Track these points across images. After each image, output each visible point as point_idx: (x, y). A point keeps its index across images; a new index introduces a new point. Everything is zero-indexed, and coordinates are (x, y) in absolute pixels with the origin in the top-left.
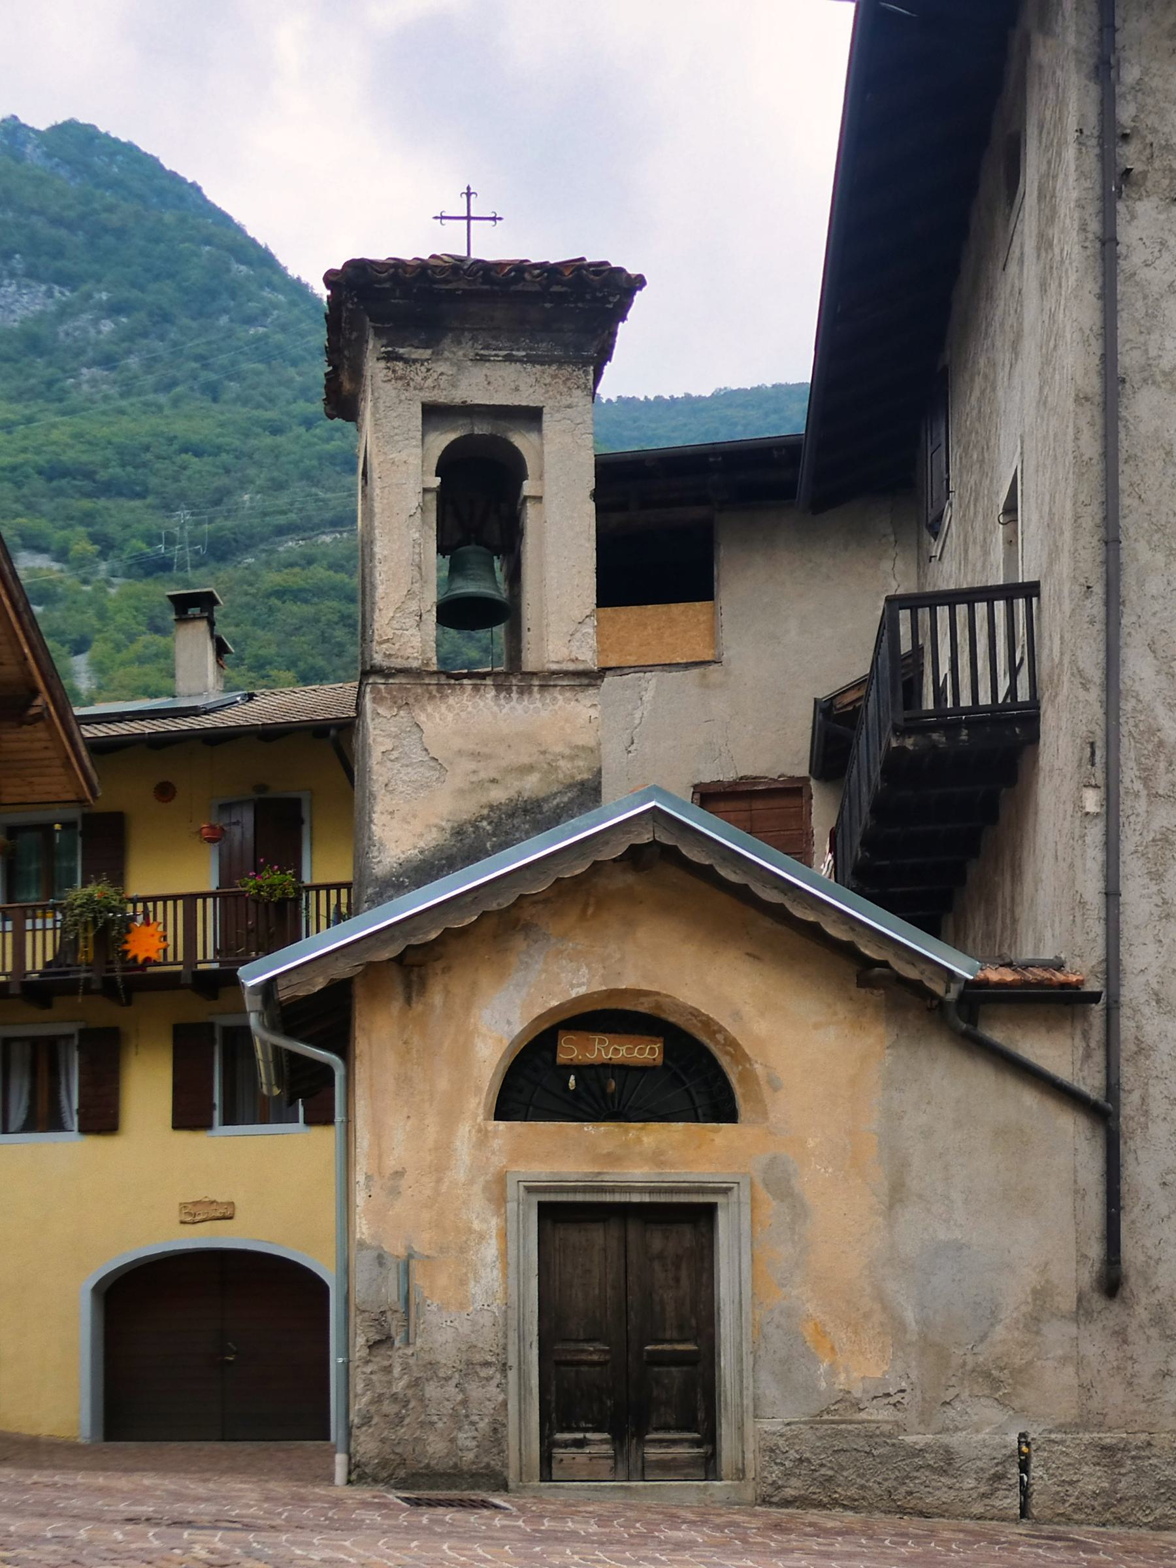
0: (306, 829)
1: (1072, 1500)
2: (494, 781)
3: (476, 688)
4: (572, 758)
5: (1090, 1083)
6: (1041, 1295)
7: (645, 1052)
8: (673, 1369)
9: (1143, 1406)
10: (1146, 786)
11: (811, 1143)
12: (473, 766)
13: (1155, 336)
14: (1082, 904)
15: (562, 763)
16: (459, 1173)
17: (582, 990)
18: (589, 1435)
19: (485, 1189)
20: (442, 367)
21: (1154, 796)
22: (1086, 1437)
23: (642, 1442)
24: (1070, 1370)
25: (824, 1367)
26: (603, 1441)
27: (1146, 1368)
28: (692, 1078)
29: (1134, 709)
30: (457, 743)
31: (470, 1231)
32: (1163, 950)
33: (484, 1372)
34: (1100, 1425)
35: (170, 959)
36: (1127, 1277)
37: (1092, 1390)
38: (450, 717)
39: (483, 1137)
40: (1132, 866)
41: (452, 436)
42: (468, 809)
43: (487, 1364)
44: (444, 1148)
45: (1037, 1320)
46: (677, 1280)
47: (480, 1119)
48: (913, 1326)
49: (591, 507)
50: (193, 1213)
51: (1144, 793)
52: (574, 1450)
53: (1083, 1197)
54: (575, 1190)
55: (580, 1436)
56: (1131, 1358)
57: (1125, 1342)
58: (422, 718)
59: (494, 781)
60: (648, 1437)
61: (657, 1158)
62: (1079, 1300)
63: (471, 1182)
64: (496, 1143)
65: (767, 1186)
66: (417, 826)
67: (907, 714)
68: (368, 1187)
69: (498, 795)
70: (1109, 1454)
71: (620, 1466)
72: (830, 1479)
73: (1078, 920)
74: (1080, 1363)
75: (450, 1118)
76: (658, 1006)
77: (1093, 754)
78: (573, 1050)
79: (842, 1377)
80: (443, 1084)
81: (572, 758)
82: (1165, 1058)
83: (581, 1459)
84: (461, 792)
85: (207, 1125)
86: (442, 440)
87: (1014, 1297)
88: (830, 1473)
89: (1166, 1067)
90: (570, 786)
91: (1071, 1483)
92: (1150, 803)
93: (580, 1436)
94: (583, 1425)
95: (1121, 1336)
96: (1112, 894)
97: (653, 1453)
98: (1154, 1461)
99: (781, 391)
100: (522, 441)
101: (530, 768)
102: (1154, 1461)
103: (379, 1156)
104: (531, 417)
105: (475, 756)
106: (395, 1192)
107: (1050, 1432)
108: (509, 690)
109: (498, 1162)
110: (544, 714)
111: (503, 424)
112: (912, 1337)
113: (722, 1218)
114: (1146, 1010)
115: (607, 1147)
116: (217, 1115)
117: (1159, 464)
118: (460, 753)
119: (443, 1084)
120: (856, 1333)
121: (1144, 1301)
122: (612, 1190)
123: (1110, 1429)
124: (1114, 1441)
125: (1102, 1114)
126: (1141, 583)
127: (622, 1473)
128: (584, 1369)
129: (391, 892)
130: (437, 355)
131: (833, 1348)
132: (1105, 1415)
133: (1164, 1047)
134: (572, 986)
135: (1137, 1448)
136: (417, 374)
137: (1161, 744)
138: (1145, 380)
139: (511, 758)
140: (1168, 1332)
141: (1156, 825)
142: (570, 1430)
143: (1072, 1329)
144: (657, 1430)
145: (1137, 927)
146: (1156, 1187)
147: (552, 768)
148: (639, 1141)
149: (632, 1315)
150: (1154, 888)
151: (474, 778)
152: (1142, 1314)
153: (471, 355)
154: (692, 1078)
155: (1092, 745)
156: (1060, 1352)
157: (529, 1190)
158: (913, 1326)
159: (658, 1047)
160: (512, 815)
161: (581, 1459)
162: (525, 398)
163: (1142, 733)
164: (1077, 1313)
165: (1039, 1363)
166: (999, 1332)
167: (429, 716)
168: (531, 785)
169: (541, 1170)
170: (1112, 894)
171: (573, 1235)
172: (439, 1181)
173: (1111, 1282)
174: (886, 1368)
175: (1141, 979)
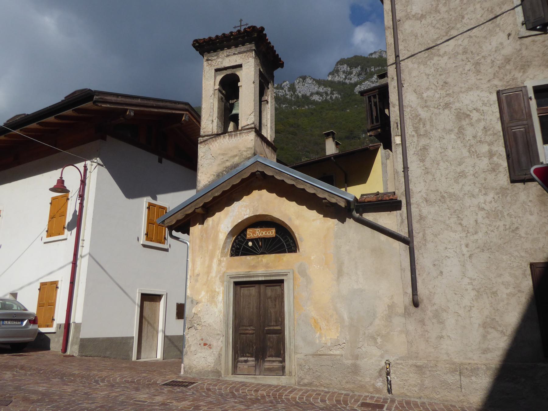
1: (407, 387)
2: (227, 160)
3: (224, 137)
4: (246, 151)
5: (404, 233)
6: (391, 307)
7: (271, 233)
8: (274, 335)
9: (433, 350)
10: (416, 133)
11: (312, 258)
12: (222, 157)
13: (409, 7)
14: (397, 172)
16: (213, 274)
17: (247, 216)
18: (249, 359)
20: (220, 60)
21: (419, 136)
22: (411, 362)
23: (264, 361)
24: (404, 336)
26: (252, 361)
28: (283, 240)
29: (410, 110)
31: (215, 291)
32: (427, 184)
33: (218, 337)
34: (417, 357)
36: (423, 300)
37: (413, 344)
39: (220, 262)
41: (223, 76)
42: (221, 169)
43: (218, 334)
44: (210, 267)
45: (390, 317)
46: (275, 305)
47: (219, 257)
51: (416, 135)
52: (244, 363)
53: (404, 272)
54: (243, 277)
55: (246, 359)
56: (427, 331)
57: (424, 325)
59: (227, 160)
60: (266, 359)
61: (267, 266)
62: (405, 309)
63: (216, 276)
64: (223, 264)
65: (299, 273)
66: (208, 175)
67: (372, 125)
68: (190, 279)
69: (228, 164)
70: (420, 369)
71: (257, 369)
72: (319, 376)
73: (396, 178)
74: (407, 333)
77: (397, 126)
78: (252, 233)
79: (324, 338)
80: (210, 247)
81: (246, 151)
82: (431, 220)
83: (246, 367)
84: (219, 165)
86: (219, 78)
87: (381, 309)
88: (319, 374)
89: (431, 224)
91: (406, 380)
92: (418, 138)
93: (246, 359)
94: (247, 355)
95: (422, 322)
96: (406, 169)
97: (267, 365)
98: (438, 372)
101: (236, 156)
102: (438, 372)
104: (240, 66)
106: (197, 281)
107: (397, 360)
108: (232, 136)
111: (234, 70)
113: (285, 284)
114: (423, 205)
115: (253, 263)
117: (414, 40)
118: (219, 154)
119: (210, 247)
120: (328, 322)
121: (430, 309)
122: (253, 277)
123: (421, 359)
124: (421, 364)
126: (410, 73)
127: (257, 373)
128: (248, 335)
130: (218, 57)
131: (320, 328)
132: (418, 353)
133: (430, 217)
134: (245, 215)
135: (431, 367)
136: (214, 63)
137: (420, 119)
138: (407, 19)
139: (231, 154)
140: (441, 321)
141: (421, 144)
142: (243, 356)
143: (403, 320)
144: (269, 357)
145: (417, 178)
146: (431, 266)
147: (242, 155)
148: (262, 260)
149: (261, 318)
150: (422, 164)
151: (222, 160)
152: (429, 313)
153: (226, 55)
154: (283, 240)
155: (397, 123)
156: (399, 329)
157: (231, 278)
159: (274, 231)
161: (246, 367)
163: (413, 117)
164: (405, 314)
165: (392, 333)
166: (377, 322)
167: (213, 146)
170: (406, 169)
171: (245, 291)
172: (208, 276)
173: (416, 304)
174: (338, 335)
175: (420, 194)
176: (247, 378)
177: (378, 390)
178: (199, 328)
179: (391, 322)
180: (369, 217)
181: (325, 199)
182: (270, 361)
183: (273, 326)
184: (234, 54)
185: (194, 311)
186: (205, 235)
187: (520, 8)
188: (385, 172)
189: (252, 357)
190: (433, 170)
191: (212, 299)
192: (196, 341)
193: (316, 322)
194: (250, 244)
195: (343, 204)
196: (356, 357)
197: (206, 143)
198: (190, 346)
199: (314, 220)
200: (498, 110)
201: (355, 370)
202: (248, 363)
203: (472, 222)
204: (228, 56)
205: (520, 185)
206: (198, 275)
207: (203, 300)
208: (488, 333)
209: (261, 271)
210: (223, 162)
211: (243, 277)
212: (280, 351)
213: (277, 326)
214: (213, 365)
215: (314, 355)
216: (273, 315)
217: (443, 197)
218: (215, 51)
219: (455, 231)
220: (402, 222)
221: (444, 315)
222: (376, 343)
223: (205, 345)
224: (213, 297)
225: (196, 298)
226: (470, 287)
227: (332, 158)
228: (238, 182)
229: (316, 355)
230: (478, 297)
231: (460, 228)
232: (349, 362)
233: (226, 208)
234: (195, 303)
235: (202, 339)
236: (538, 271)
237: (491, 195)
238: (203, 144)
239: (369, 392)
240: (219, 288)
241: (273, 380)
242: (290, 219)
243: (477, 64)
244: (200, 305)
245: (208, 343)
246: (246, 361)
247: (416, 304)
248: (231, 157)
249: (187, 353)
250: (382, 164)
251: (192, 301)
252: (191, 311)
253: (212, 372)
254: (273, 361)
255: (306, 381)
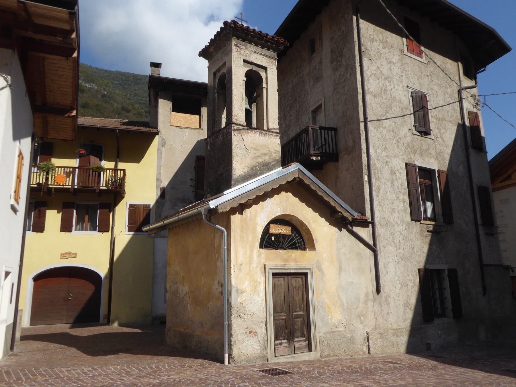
0: (103, 154)
4: (275, 153)
5: (371, 243)
6: (367, 294)
7: (286, 230)
8: (299, 320)
12: (255, 152)
15: (273, 154)
16: (254, 265)
19: (260, 269)
20: (247, 52)
23: (294, 342)
25: (330, 317)
26: (286, 343)
27: (385, 312)
30: (251, 145)
35: (67, 184)
38: (250, 138)
40: (374, 193)
42: (254, 163)
44: (251, 257)
46: (299, 294)
48: (345, 304)
49: (277, 93)
50: (64, 256)
54: (280, 269)
55: (280, 341)
58: (244, 137)
63: (257, 267)
64: (262, 256)
68: (234, 269)
69: (260, 160)
75: (252, 248)
76: (291, 219)
78: (275, 229)
85: (70, 231)
87: (362, 297)
90: (275, 160)
97: (297, 345)
99: (145, 76)
100: (263, 74)
101: (266, 154)
103: (236, 260)
105: (255, 149)
106: (240, 270)
109: (263, 261)
110: (269, 141)
112: (345, 307)
115: (285, 257)
116: (74, 228)
119: (250, 238)
122: (287, 269)
125: (373, 248)
128: (281, 321)
129: (237, 183)
133: (382, 235)
136: (242, 51)
137: (376, 167)
148: (291, 255)
158: (345, 304)
160: (263, 166)
162: (264, 64)
168: (267, 158)
169: (271, 264)
172: (250, 267)
176: (287, 358)
177: (364, 353)
178: (245, 317)
179: (367, 305)
180: (355, 229)
181: (341, 212)
182: (298, 341)
183: (298, 311)
184: (261, 54)
185: (239, 300)
186: (244, 225)
187: (412, 116)
188: (159, 157)
189: (284, 339)
190: (382, 204)
191: (255, 289)
192: (242, 330)
193: (329, 307)
194: (273, 238)
195: (350, 219)
196: (351, 331)
197: (239, 132)
198: (237, 336)
199: (324, 226)
200: (405, 174)
201: (352, 340)
202: (283, 345)
203: (398, 241)
204: (255, 52)
205: (413, 222)
206: (241, 265)
207: (247, 290)
208: (406, 309)
209: (292, 264)
210: (256, 157)
211: (280, 269)
212: (307, 332)
213: (300, 311)
214: (259, 351)
215: (330, 333)
216: (298, 302)
217: (387, 223)
218: (244, 40)
219: (392, 246)
220: (370, 236)
221: (389, 299)
222: (361, 319)
223: (250, 332)
224: (256, 287)
225: (240, 287)
226: (398, 282)
227: (118, 131)
228: (284, 183)
229: (331, 332)
230: (401, 287)
231: (393, 245)
232: (349, 335)
233: (261, 203)
234: (240, 292)
235: (247, 328)
236: (422, 273)
237: (405, 226)
238: (237, 132)
239: (360, 355)
240: (261, 278)
241: (306, 356)
242: (309, 222)
243: (398, 141)
244: (244, 294)
245: (254, 331)
246: (281, 344)
247: (378, 291)
248: (262, 154)
249: (235, 342)
250: (158, 150)
251: (237, 290)
252: (237, 301)
253: (260, 357)
254: (300, 341)
255: (326, 353)
